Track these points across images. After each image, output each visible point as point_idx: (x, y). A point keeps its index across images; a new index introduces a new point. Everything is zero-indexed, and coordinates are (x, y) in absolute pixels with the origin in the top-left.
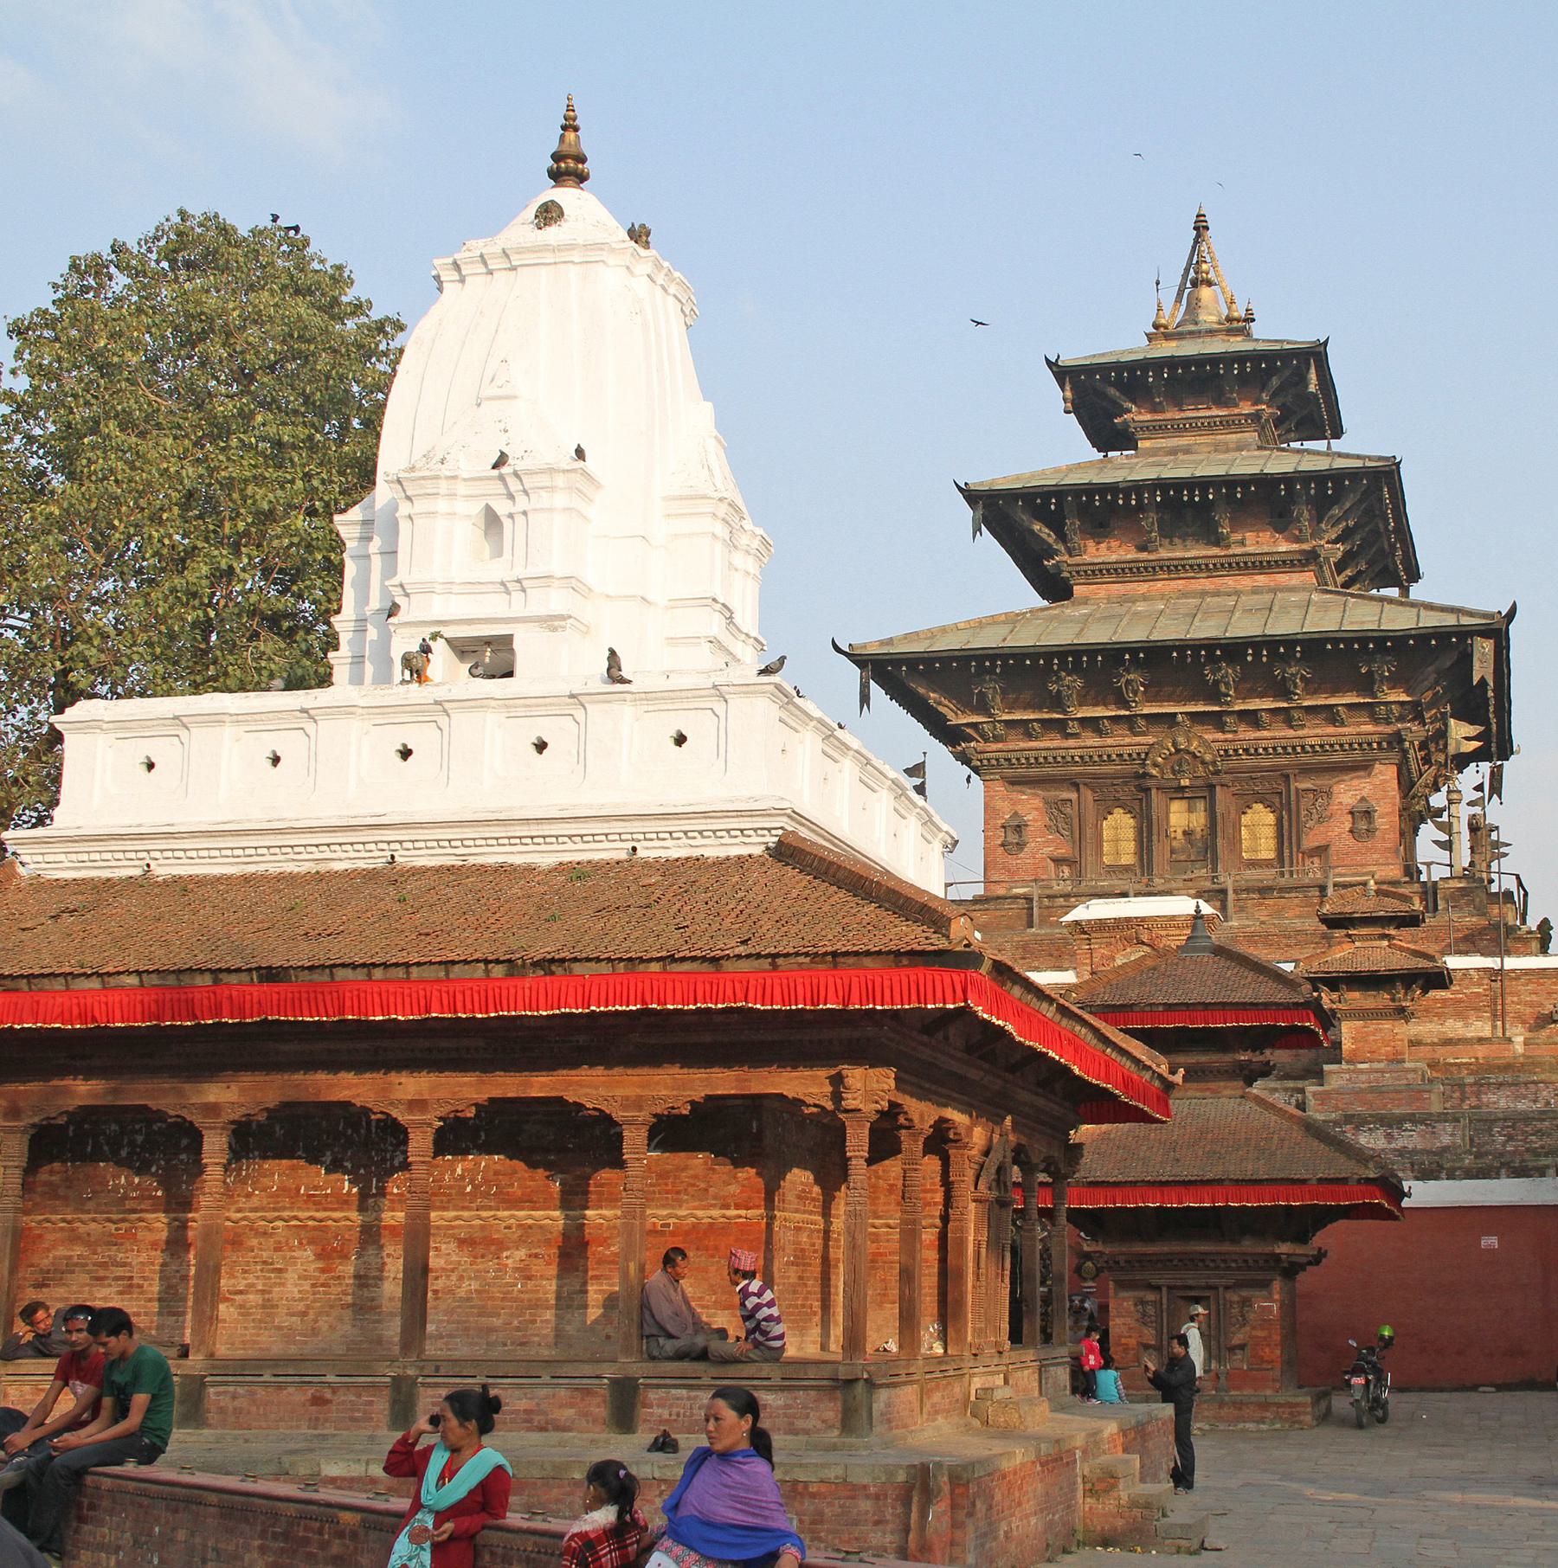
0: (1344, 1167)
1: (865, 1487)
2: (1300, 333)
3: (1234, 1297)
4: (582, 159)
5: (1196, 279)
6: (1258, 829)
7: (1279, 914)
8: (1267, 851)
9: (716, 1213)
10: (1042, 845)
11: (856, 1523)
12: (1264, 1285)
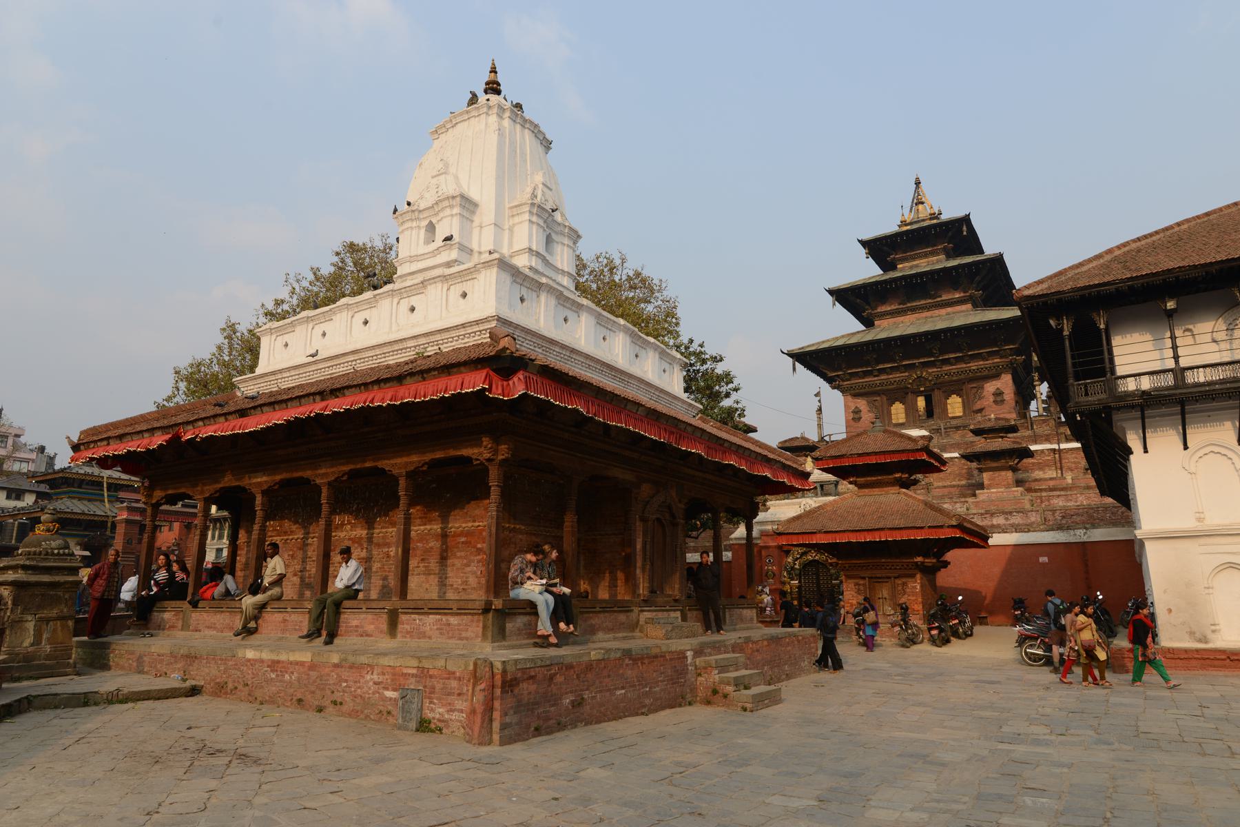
0: (941, 520)
1: (454, 673)
2: (959, 214)
3: (899, 582)
4: (499, 84)
6: (955, 405)
7: (963, 436)
9: (470, 524)
10: (867, 416)
11: (449, 694)
12: (913, 576)
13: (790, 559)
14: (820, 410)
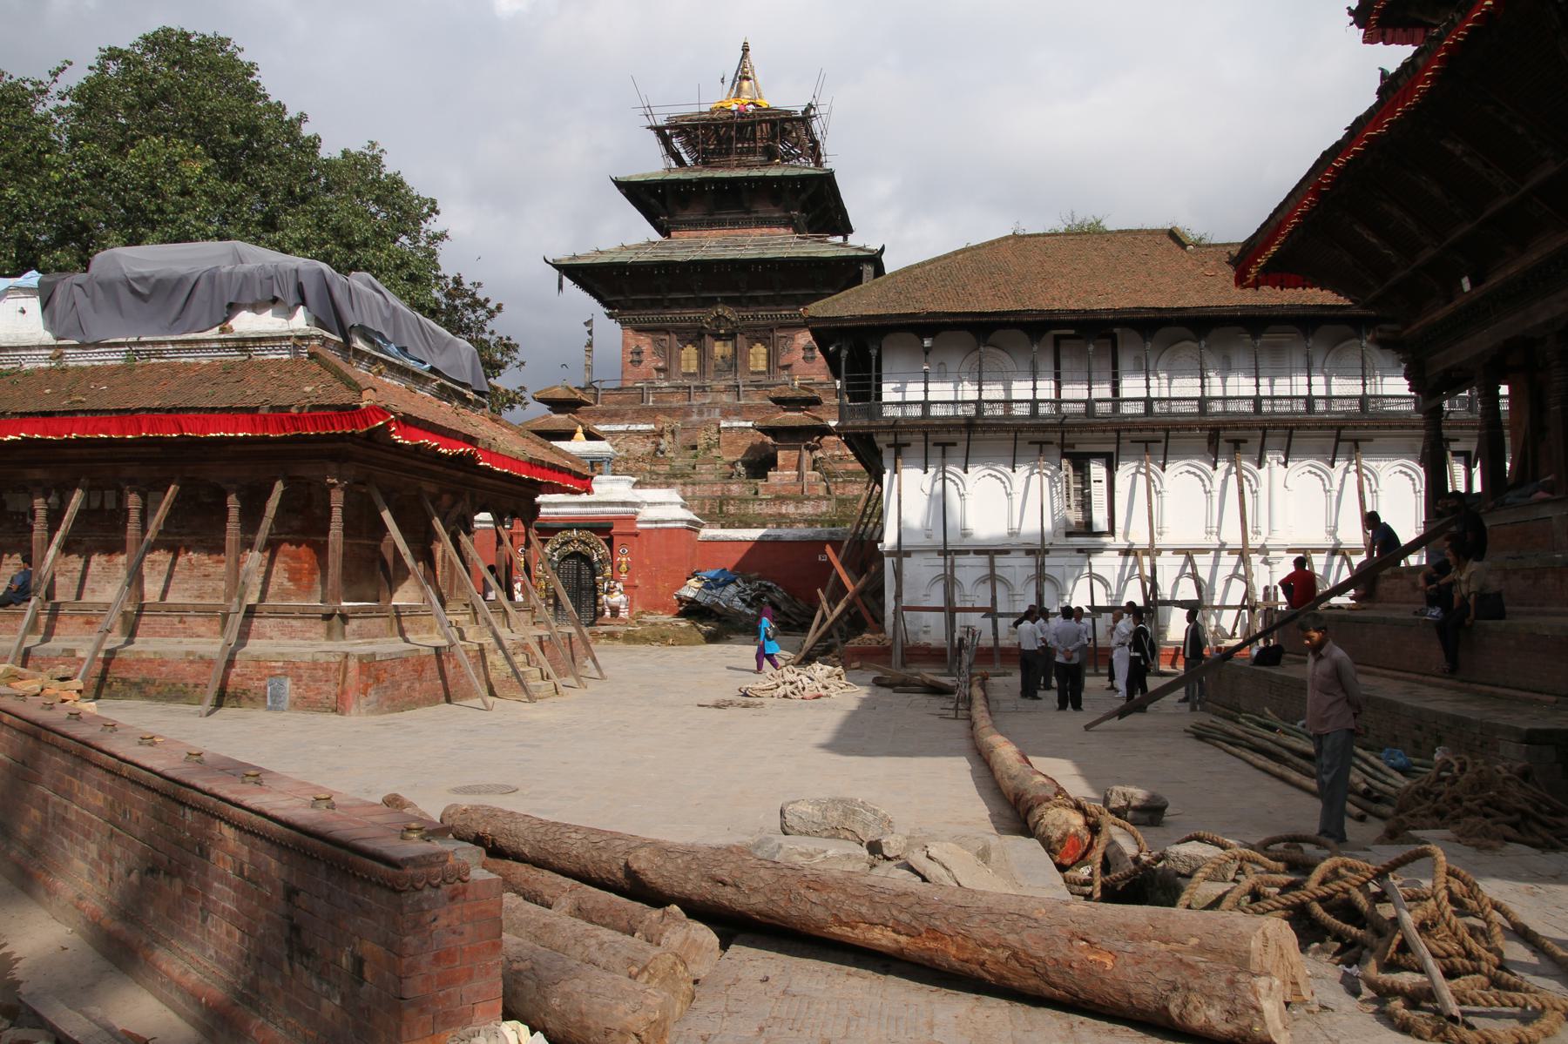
5: (743, 76)
8: (762, 366)
10: (651, 361)
13: (547, 550)
14: (590, 345)
